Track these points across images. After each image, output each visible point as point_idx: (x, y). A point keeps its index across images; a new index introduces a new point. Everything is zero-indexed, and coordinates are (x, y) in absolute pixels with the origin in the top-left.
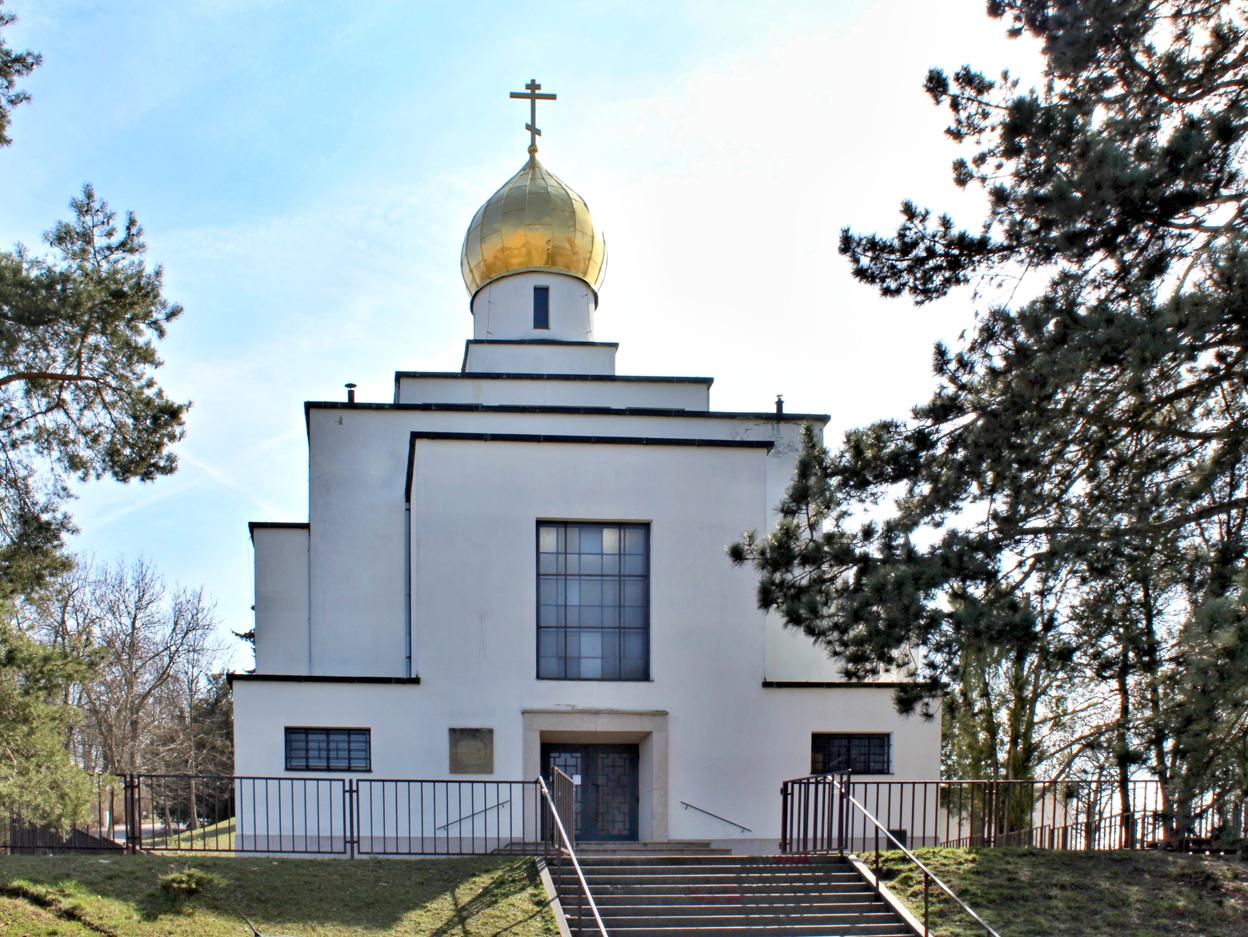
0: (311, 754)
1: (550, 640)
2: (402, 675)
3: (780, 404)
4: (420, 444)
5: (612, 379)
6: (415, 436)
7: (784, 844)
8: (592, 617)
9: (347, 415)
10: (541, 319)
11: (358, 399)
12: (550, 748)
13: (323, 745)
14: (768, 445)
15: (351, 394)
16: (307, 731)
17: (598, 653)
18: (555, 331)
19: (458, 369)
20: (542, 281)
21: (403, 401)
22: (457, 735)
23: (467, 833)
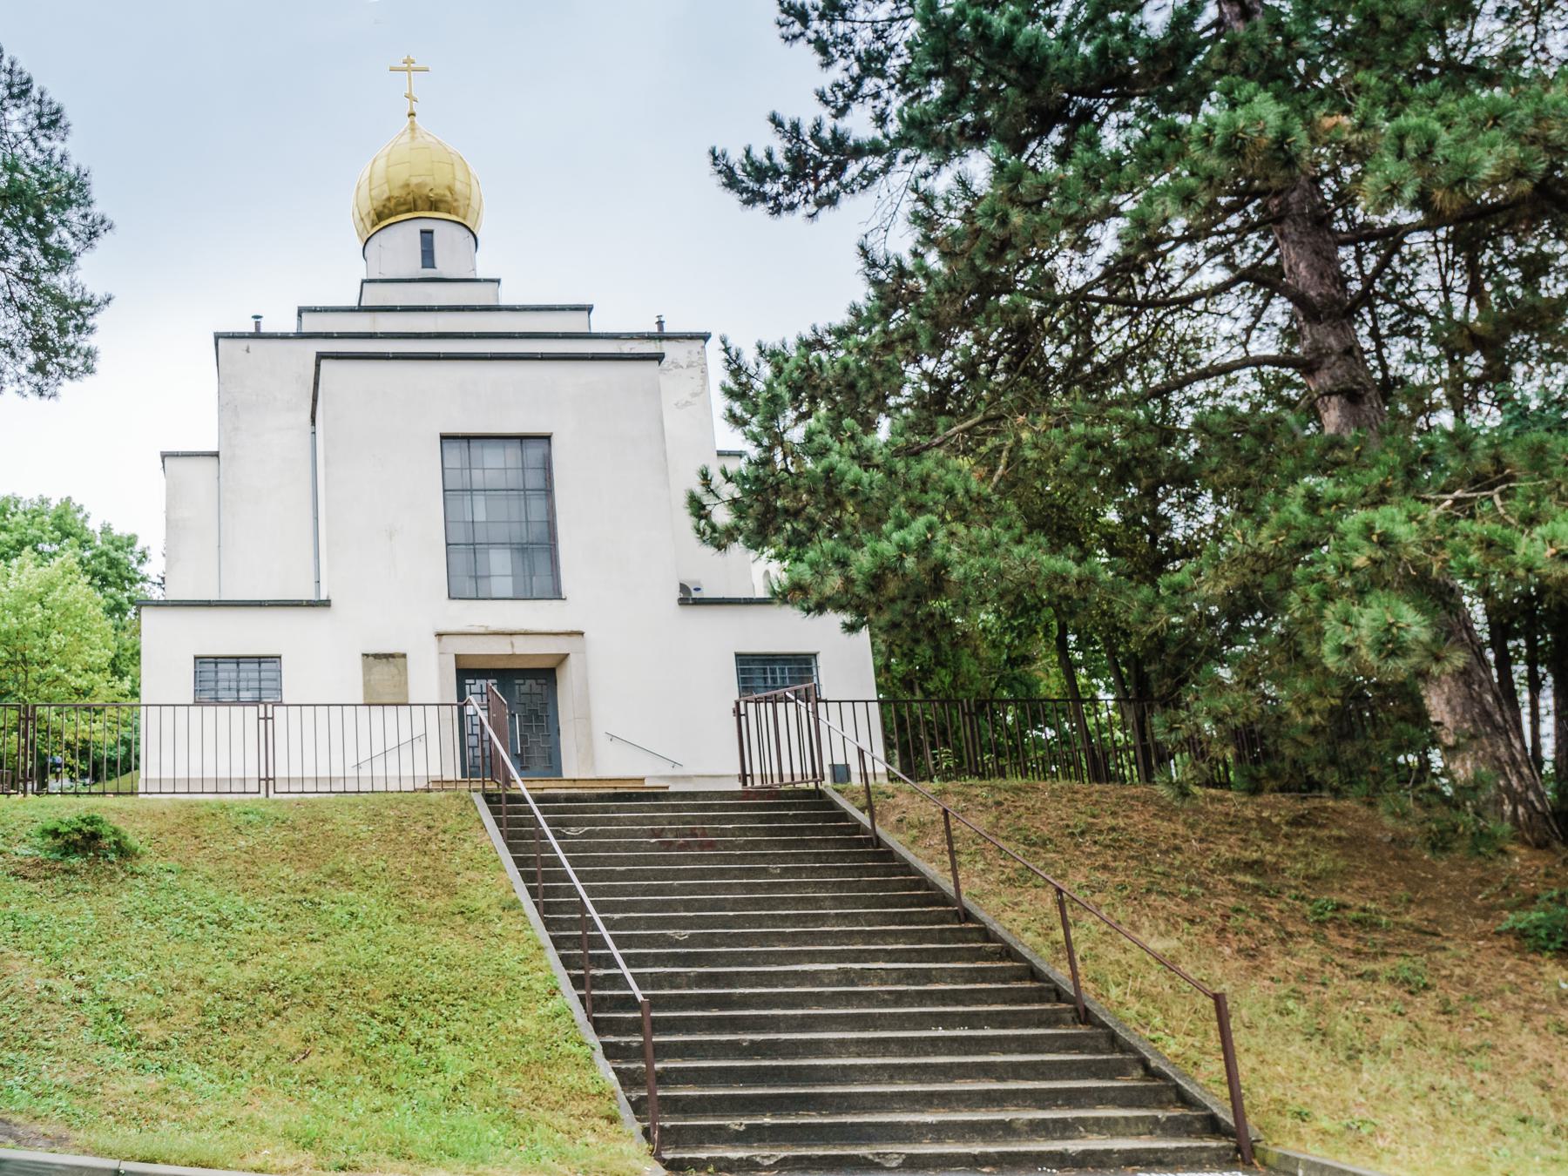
0: (221, 685)
1: (461, 558)
2: (312, 597)
3: (660, 323)
4: (324, 363)
5: (498, 309)
6: (321, 356)
7: (743, 777)
8: (500, 533)
9: (253, 344)
10: (428, 257)
11: (263, 330)
12: (466, 672)
13: (233, 675)
14: (659, 358)
15: (257, 325)
16: (217, 660)
17: (509, 572)
18: (443, 267)
19: (355, 303)
20: (427, 225)
21: (305, 330)
22: (375, 658)
23: (379, 772)
